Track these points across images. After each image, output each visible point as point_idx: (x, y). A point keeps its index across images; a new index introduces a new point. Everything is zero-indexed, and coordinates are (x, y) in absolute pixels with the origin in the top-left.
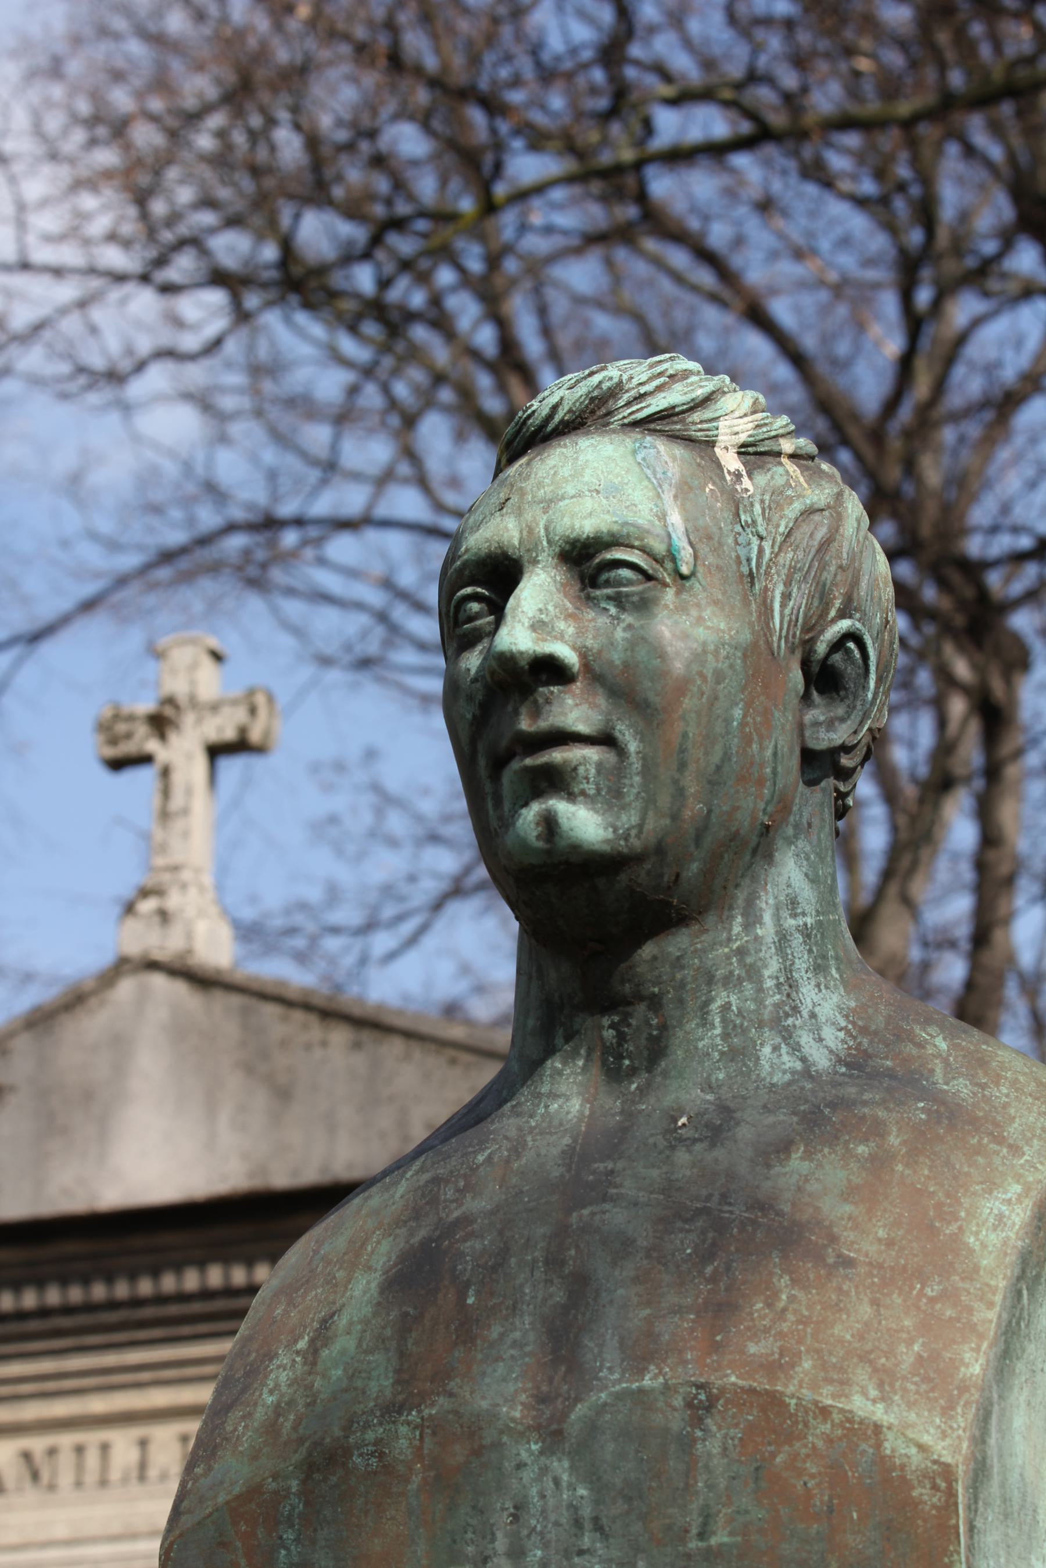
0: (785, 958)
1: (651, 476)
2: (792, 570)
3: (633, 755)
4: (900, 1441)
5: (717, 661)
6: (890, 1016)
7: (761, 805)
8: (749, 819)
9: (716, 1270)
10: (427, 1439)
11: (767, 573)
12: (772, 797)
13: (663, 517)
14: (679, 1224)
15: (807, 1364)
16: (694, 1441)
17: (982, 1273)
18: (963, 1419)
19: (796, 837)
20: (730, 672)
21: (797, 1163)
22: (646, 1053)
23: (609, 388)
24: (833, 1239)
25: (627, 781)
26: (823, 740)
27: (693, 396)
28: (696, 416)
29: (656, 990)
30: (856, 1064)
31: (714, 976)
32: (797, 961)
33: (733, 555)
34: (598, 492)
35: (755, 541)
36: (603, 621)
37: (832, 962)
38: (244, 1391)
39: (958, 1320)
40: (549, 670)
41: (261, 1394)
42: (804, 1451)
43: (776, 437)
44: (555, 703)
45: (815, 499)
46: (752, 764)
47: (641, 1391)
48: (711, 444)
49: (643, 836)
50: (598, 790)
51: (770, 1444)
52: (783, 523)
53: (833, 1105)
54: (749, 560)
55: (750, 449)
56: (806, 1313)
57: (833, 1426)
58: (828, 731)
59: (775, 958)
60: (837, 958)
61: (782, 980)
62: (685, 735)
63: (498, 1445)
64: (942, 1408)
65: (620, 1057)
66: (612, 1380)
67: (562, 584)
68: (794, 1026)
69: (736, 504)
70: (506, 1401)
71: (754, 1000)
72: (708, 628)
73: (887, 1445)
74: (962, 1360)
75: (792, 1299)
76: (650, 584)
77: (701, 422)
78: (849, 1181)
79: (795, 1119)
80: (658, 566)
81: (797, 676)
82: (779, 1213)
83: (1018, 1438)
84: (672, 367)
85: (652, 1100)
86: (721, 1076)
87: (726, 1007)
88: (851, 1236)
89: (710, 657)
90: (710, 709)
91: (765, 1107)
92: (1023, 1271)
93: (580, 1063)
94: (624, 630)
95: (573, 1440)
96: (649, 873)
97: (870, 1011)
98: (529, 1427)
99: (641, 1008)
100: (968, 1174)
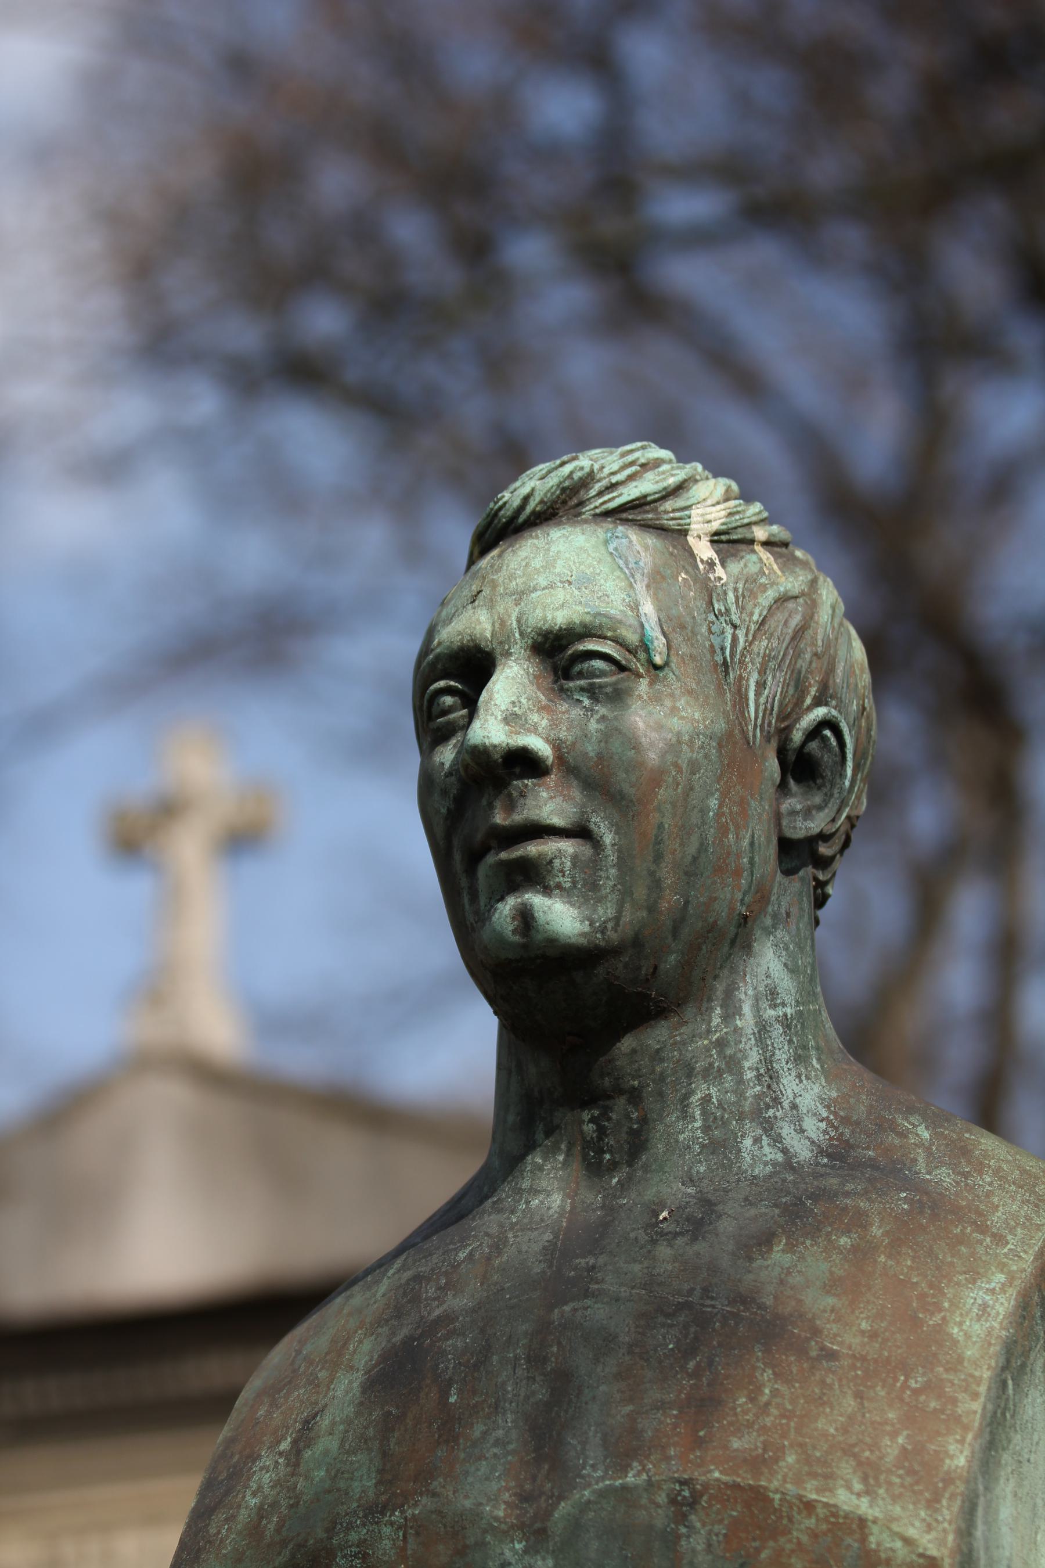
0: (764, 1048)
1: (623, 566)
2: (767, 658)
3: (609, 847)
4: (885, 1535)
5: (692, 751)
6: (871, 1106)
7: (739, 896)
8: (726, 910)
9: (698, 1365)
10: (410, 1540)
11: (741, 662)
12: (750, 887)
13: (635, 607)
14: (661, 1319)
15: (791, 1459)
16: (679, 1537)
17: (966, 1364)
18: (949, 1511)
19: (774, 927)
20: (705, 762)
21: (779, 1255)
22: (626, 1147)
23: (581, 478)
24: (816, 1332)
25: (602, 874)
26: (801, 829)
27: (665, 484)
28: (668, 505)
29: (636, 1083)
30: (837, 1154)
31: (694, 1069)
32: (777, 1052)
33: (707, 644)
34: (570, 583)
35: (729, 630)
36: (576, 712)
37: (813, 1052)
38: (227, 1493)
39: (942, 1411)
40: (522, 763)
41: (244, 1497)
42: (788, 1546)
43: (749, 524)
44: (529, 795)
45: (789, 586)
46: (729, 854)
47: (624, 1488)
48: (684, 533)
49: (619, 929)
50: (574, 883)
51: (754, 1539)
52: (757, 611)
53: (815, 1197)
54: (723, 649)
55: (723, 538)
56: (790, 1407)
57: (817, 1520)
58: (805, 820)
59: (755, 1049)
60: (818, 1048)
61: (762, 1071)
62: (661, 826)
63: (482, 1545)
64: (928, 1501)
65: (601, 1152)
66: (595, 1478)
67: (535, 677)
68: (776, 1117)
69: (709, 592)
70: (489, 1500)
71: (735, 1092)
72: (682, 718)
73: (872, 1539)
74: (946, 1452)
75: (775, 1393)
76: (622, 675)
77: (674, 511)
78: (832, 1273)
79: (777, 1211)
80: (631, 657)
81: (773, 765)
82: (762, 1307)
83: (1005, 1529)
84: (643, 456)
85: (633, 1195)
86: (702, 1169)
87: (707, 1099)
88: (834, 1328)
89: (685, 747)
90: (685, 800)
91: (746, 1199)
92: (1008, 1361)
93: (561, 1158)
94: (598, 721)
95: (557, 1539)
96: (626, 966)
97: (852, 1101)
98: (512, 1526)
99: (621, 1102)
100: (952, 1264)
